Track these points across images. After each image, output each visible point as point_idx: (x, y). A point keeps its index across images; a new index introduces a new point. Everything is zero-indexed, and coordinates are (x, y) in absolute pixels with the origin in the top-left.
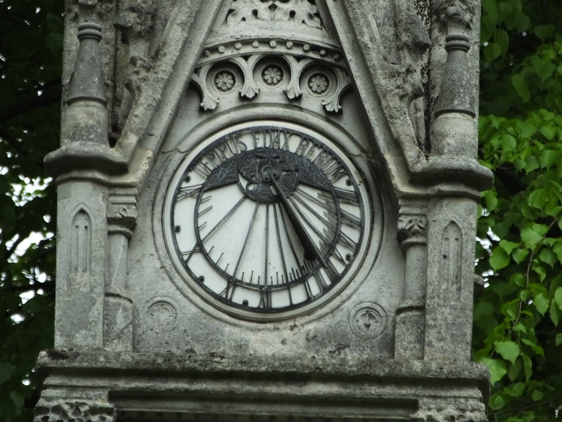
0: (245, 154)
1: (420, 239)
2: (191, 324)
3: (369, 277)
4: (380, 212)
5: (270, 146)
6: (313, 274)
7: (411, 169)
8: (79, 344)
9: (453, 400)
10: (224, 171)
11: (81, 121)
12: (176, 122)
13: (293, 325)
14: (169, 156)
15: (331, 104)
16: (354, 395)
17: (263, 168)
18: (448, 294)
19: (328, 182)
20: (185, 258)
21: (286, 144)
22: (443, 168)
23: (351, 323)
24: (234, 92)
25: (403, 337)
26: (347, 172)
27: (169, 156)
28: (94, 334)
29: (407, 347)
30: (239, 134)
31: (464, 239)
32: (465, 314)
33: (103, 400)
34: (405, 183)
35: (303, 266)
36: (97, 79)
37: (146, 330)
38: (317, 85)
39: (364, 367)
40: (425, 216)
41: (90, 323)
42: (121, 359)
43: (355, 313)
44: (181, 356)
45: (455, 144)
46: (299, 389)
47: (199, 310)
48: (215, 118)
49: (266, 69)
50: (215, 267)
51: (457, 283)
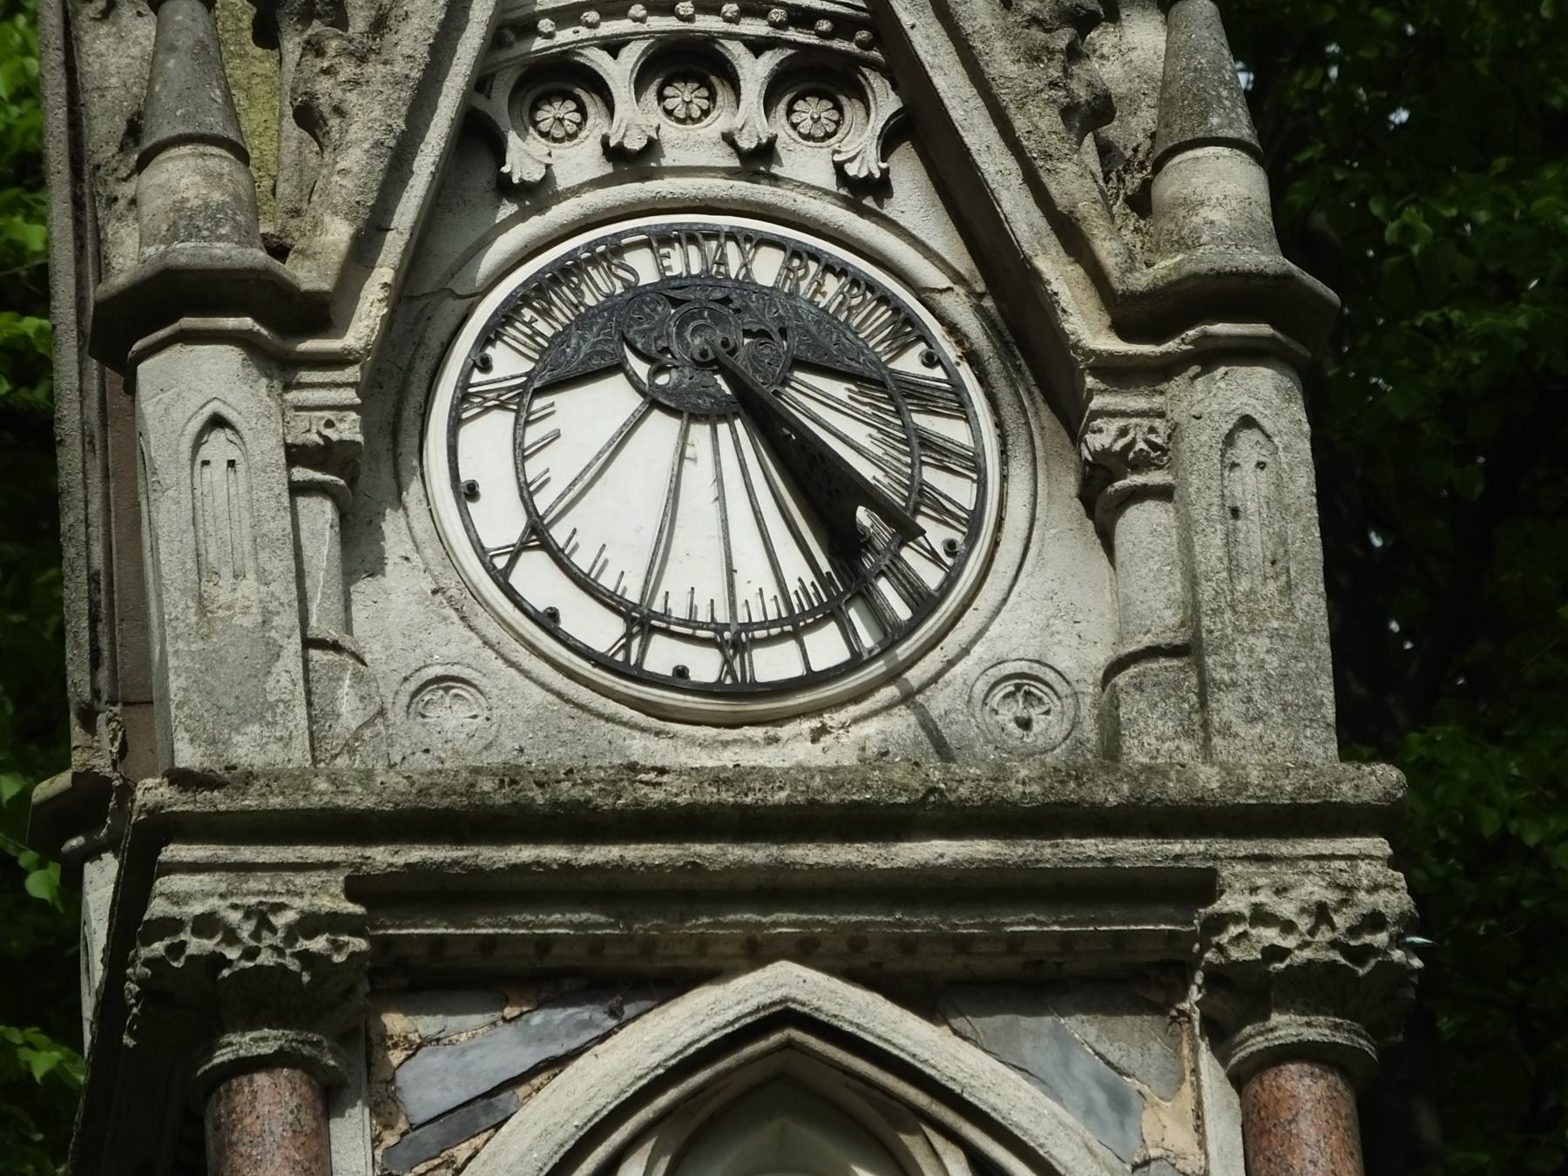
0: (636, 293)
1: (1156, 478)
3: (1012, 598)
4: (1023, 431)
8: (244, 762)
9: (1313, 865)
10: (582, 338)
11: (190, 194)
14: (426, 306)
15: (859, 158)
16: (1038, 861)
17: (690, 328)
18: (1256, 602)
20: (501, 563)
22: (1212, 270)
23: (977, 714)
24: (587, 142)
26: (924, 337)
27: (426, 306)
28: (286, 734)
29: (1158, 750)
30: (616, 249)
31: (1283, 460)
32: (1312, 649)
33: (332, 896)
36: (218, 92)
37: (409, 751)
38: (812, 118)
39: (1062, 782)
40: (1161, 415)
41: (272, 707)
46: (883, 851)
47: (551, 698)
50: (585, 584)
51: (1276, 578)
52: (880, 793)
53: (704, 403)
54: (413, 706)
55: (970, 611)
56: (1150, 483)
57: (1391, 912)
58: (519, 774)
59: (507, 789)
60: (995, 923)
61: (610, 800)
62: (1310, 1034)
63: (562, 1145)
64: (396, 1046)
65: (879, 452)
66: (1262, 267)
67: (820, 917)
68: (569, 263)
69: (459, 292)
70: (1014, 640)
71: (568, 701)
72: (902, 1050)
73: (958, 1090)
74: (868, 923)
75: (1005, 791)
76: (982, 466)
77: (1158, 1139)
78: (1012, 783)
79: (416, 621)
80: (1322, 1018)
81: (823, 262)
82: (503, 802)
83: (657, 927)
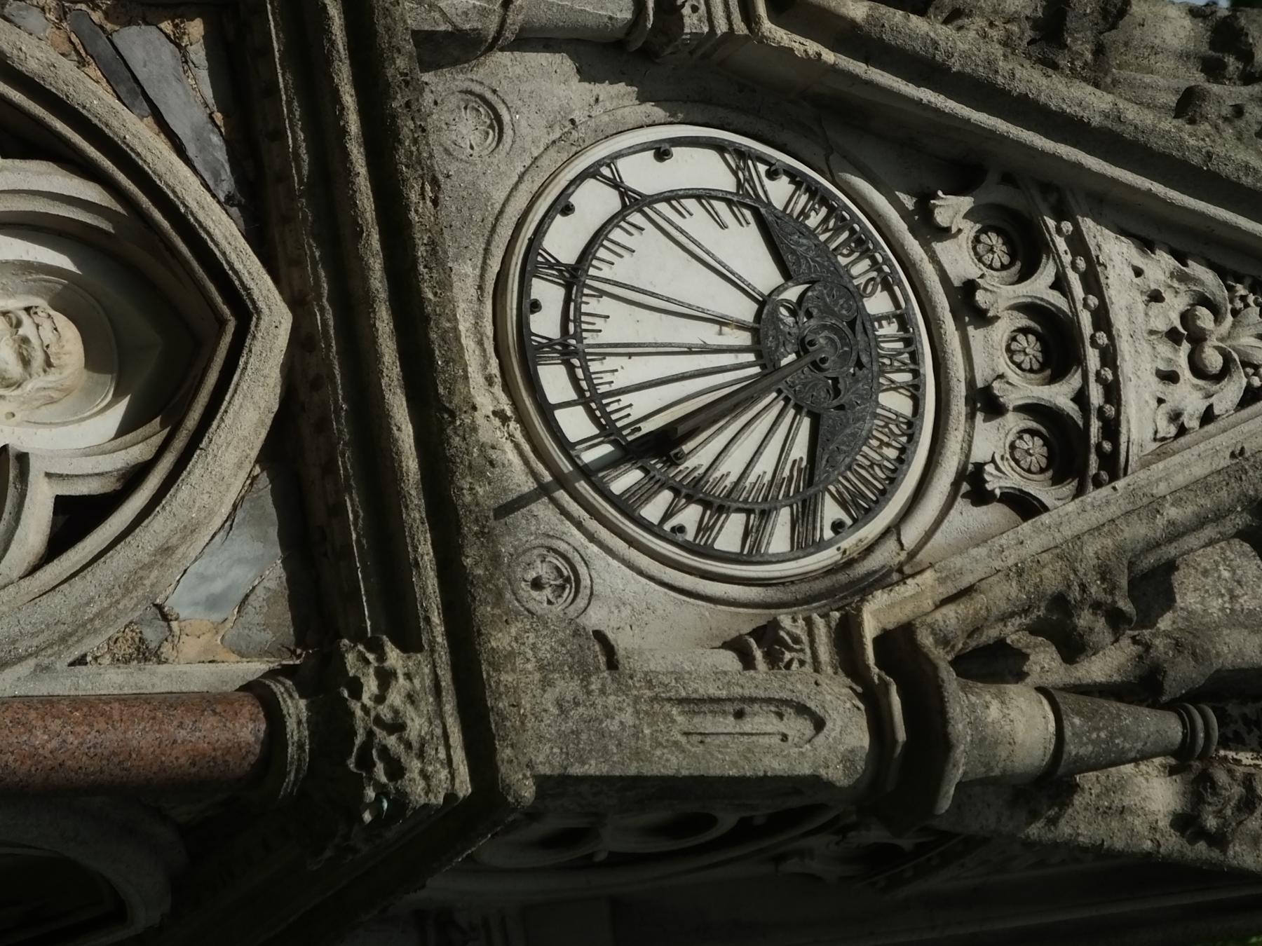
0: (857, 295)
3: (644, 581)
10: (809, 248)
15: (1000, 474)
16: (407, 507)
17: (832, 336)
20: (606, 171)
22: (943, 681)
29: (524, 644)
35: (639, 429)
37: (434, 89)
44: (419, 111)
45: (989, 720)
46: (396, 383)
47: (498, 207)
49: (1039, 338)
52: (444, 373)
53: (770, 343)
54: (473, 98)
57: (403, 783)
58: (415, 89)
60: (351, 485)
62: (291, 724)
63: (107, 125)
64: (176, 26)
66: (952, 722)
67: (333, 344)
69: (831, 158)
71: (497, 219)
72: (230, 403)
73: (203, 445)
74: (335, 383)
75: (461, 474)
77: (188, 630)
78: (469, 479)
80: (306, 733)
82: (389, 75)
83: (305, 217)
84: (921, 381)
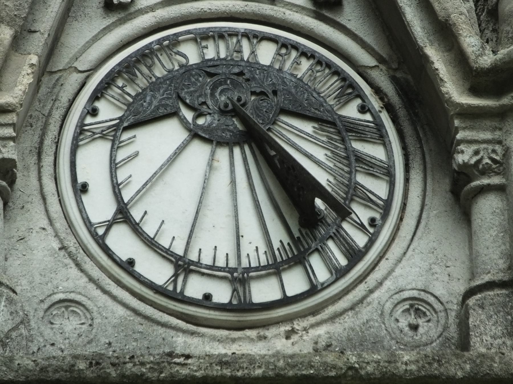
1: (496, 180)
2: (118, 333)
3: (410, 252)
4: (418, 152)
5: (227, 56)
6: (317, 250)
7: (473, 64)
10: (153, 96)
12: (67, 26)
13: (290, 329)
14: (60, 77)
17: (220, 88)
19: (329, 108)
21: (253, 52)
25: (482, 328)
26: (360, 95)
27: (60, 77)
29: (492, 344)
34: (463, 92)
35: (298, 238)
37: (43, 345)
39: (429, 364)
40: (500, 142)
42: (16, 365)
43: (391, 307)
47: (129, 313)
48: (131, 19)
55: (384, 260)
56: (492, 183)
58: (101, 358)
59: (93, 368)
61: (156, 374)
65: (331, 165)
68: (147, 51)
70: (410, 278)
76: (393, 173)
79: (49, 266)
81: (300, 51)
82: (91, 375)
84: (250, 33)
